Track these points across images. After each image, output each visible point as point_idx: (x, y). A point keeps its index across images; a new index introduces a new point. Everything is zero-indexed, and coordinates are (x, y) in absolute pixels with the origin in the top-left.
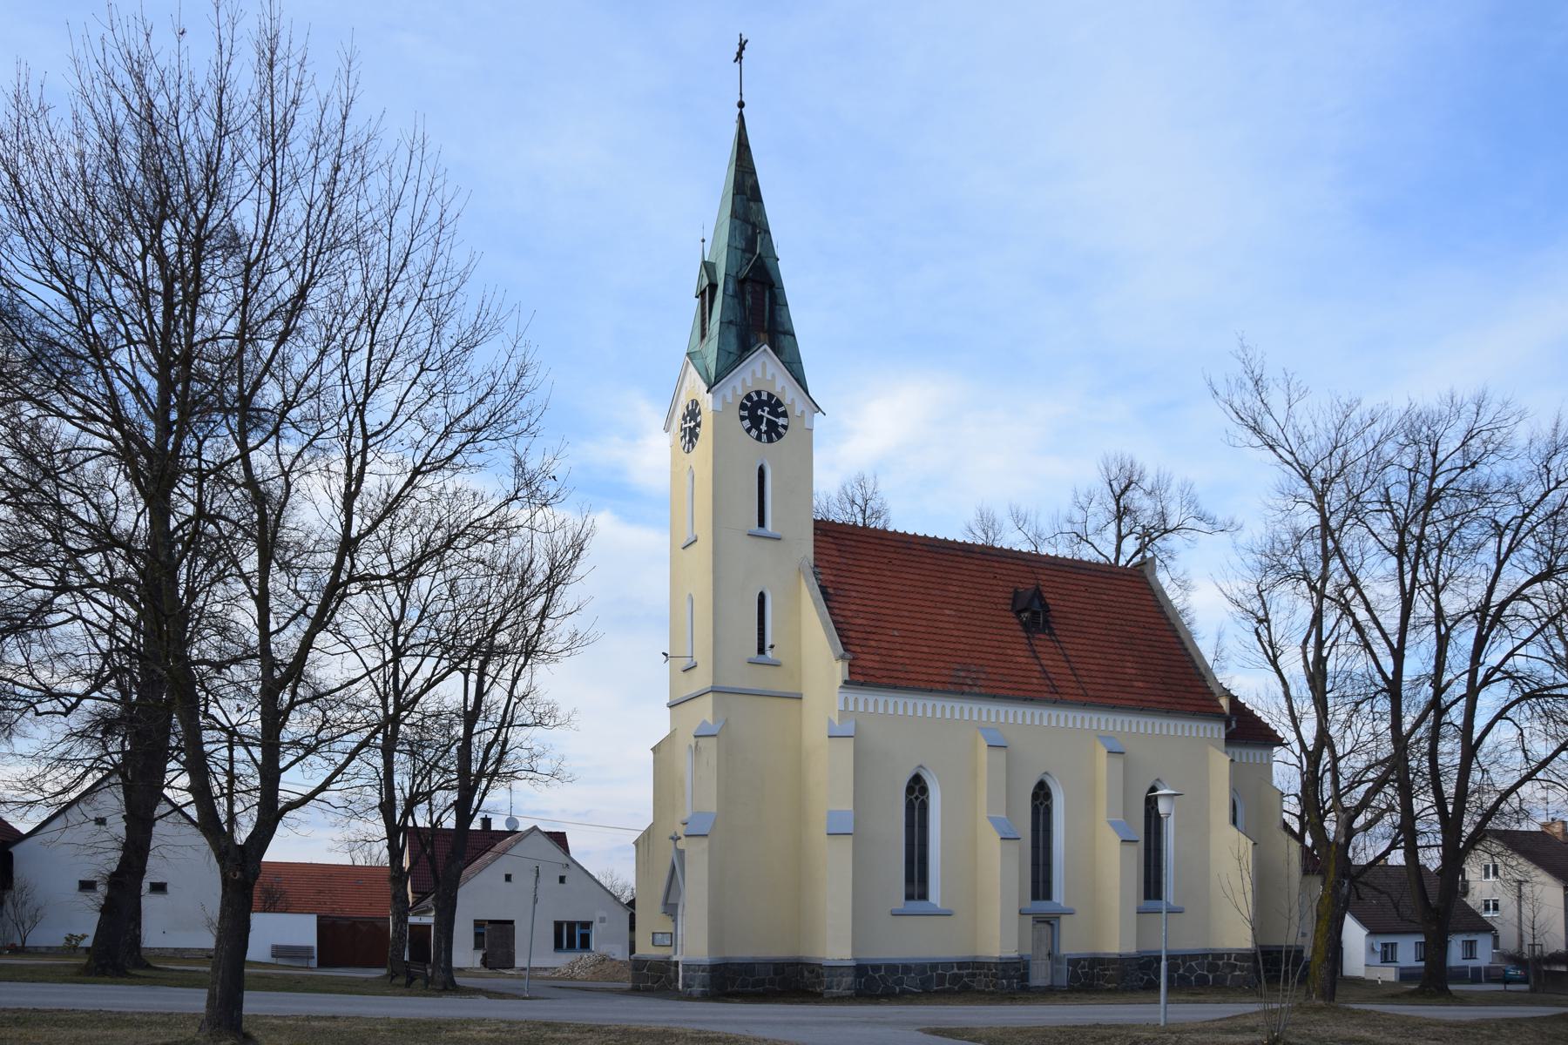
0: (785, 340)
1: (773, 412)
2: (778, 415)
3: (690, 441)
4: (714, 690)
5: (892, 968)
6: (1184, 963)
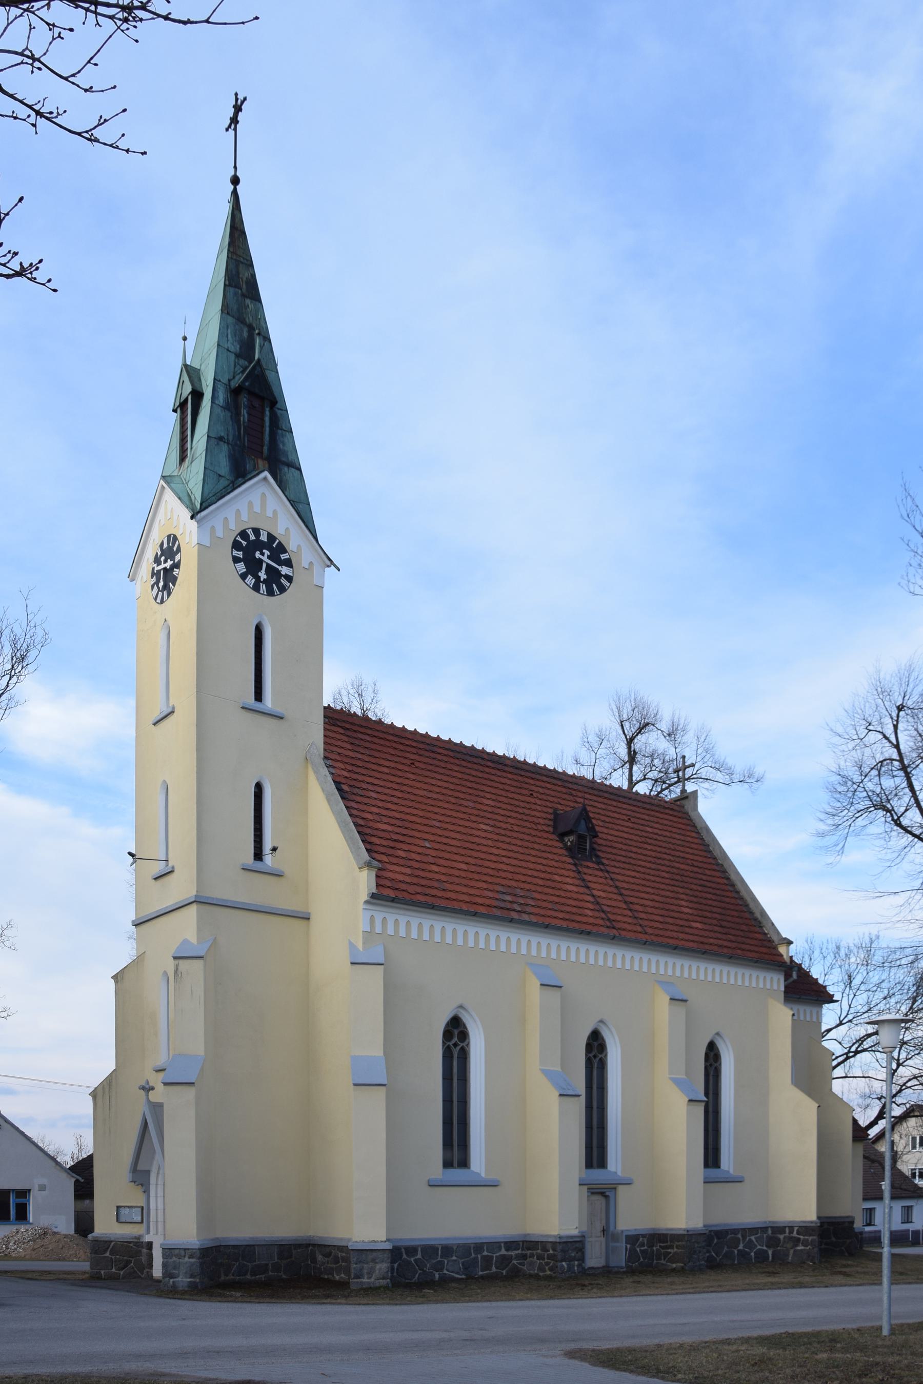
0: (290, 473)
1: (274, 557)
2: (281, 562)
3: (166, 587)
4: (198, 901)
5: (430, 1250)
6: (744, 1237)
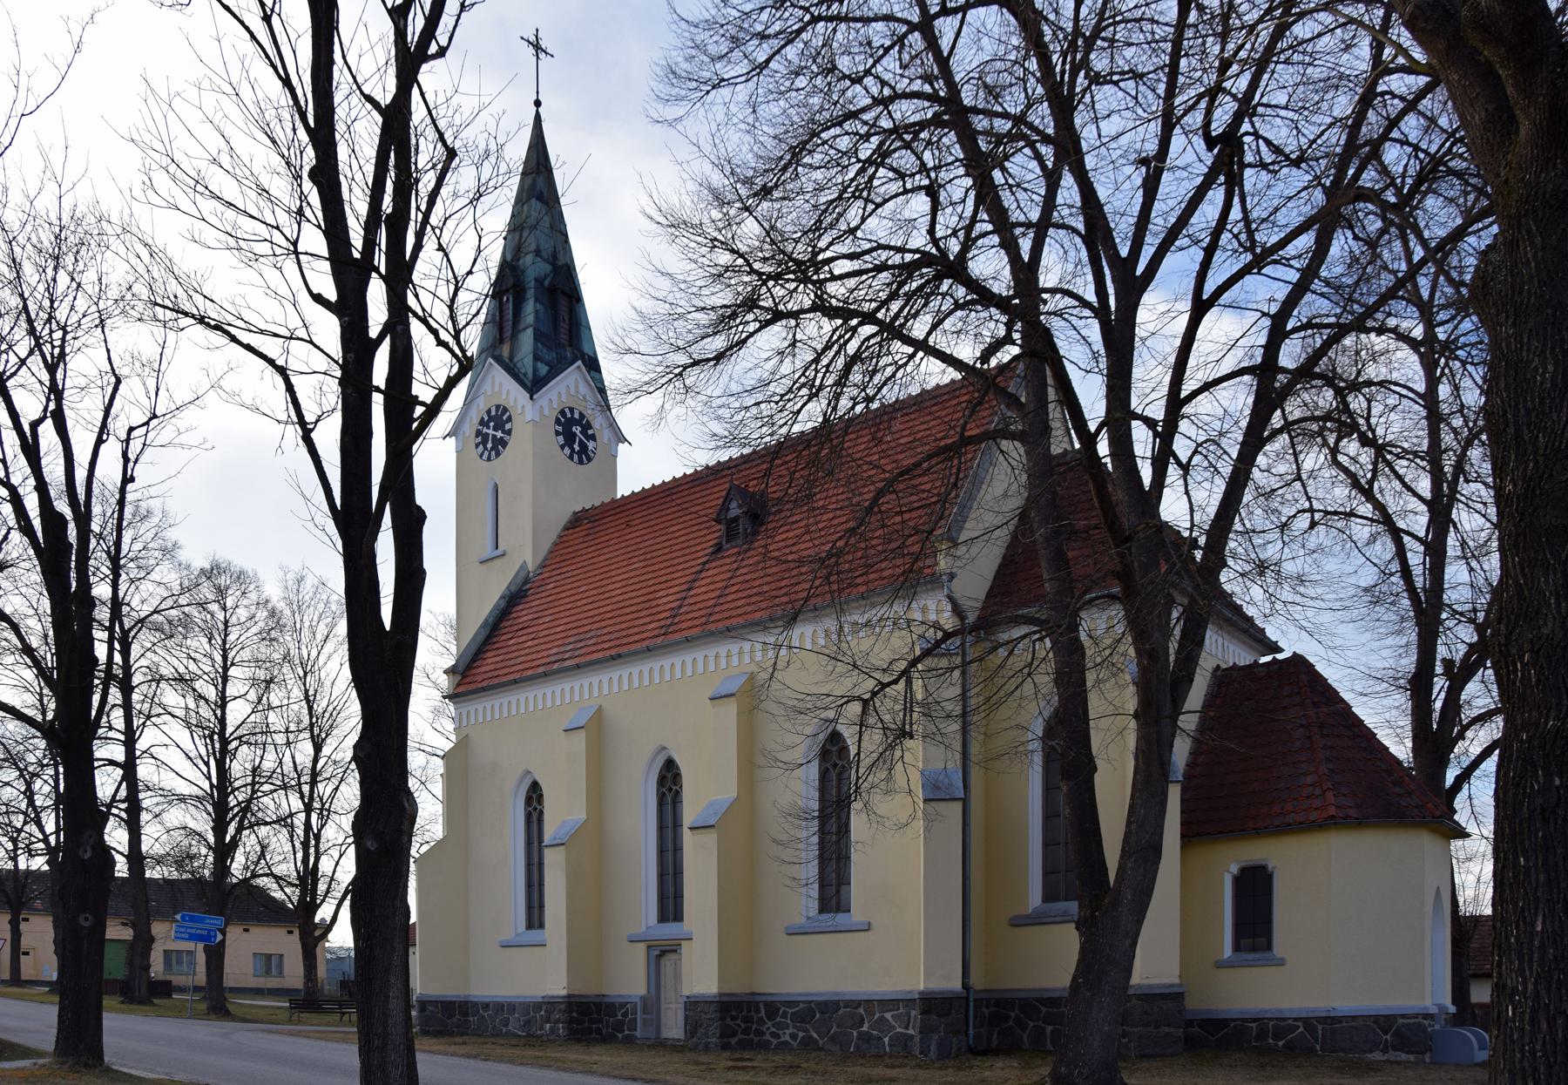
1: (584, 432)
